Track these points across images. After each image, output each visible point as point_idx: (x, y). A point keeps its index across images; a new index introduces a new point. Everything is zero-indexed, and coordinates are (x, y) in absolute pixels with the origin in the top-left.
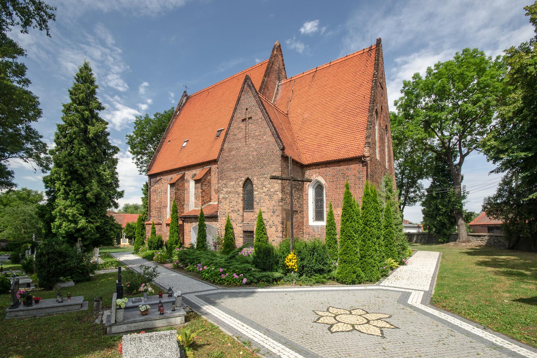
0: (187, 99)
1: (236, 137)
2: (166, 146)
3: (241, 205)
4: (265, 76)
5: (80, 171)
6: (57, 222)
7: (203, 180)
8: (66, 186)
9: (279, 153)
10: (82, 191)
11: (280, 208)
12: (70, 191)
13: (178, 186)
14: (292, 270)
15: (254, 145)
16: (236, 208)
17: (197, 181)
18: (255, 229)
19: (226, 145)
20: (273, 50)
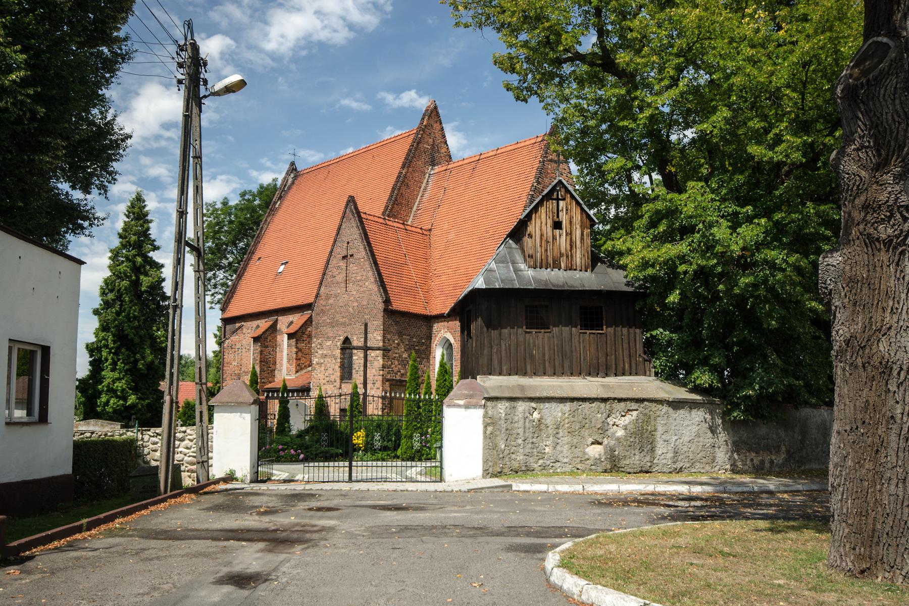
0: (296, 177)
1: (335, 280)
2: (254, 268)
3: (339, 374)
4: (403, 167)
5: (131, 336)
6: (104, 398)
7: (299, 334)
8: (114, 354)
9: (381, 306)
10: (132, 359)
11: (381, 378)
12: (119, 360)
13: (265, 340)
14: (360, 449)
15: (355, 293)
16: (332, 378)
17: (290, 336)
18: (348, 408)
19: (322, 289)
20: (423, 119)
